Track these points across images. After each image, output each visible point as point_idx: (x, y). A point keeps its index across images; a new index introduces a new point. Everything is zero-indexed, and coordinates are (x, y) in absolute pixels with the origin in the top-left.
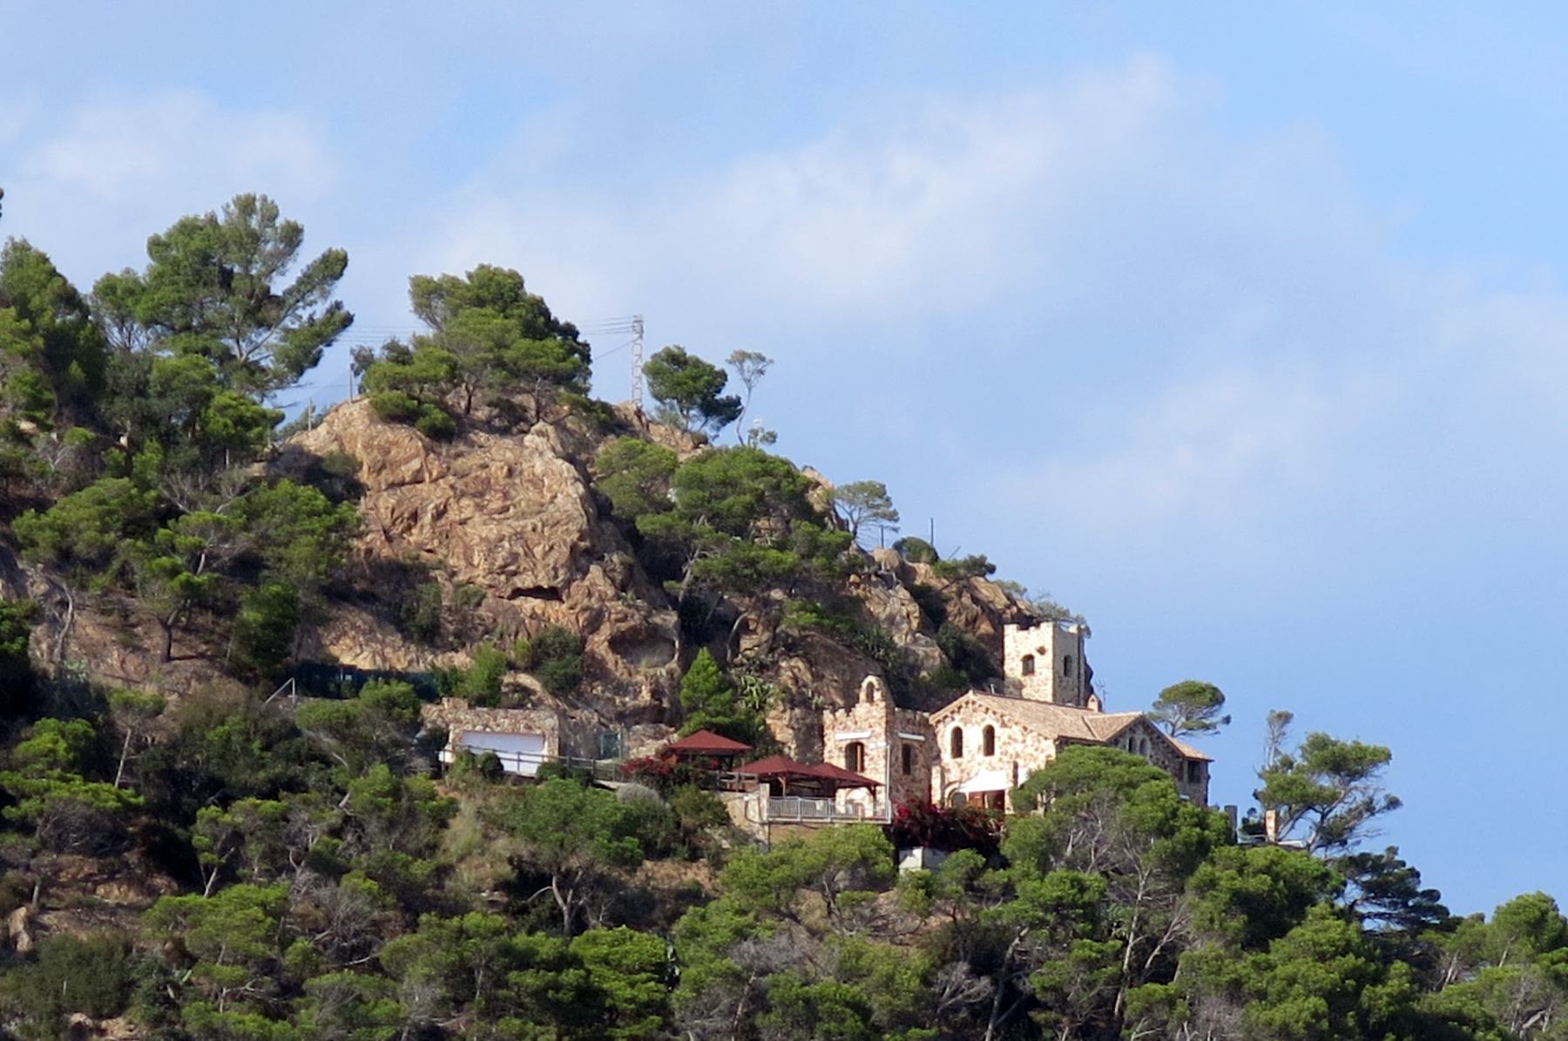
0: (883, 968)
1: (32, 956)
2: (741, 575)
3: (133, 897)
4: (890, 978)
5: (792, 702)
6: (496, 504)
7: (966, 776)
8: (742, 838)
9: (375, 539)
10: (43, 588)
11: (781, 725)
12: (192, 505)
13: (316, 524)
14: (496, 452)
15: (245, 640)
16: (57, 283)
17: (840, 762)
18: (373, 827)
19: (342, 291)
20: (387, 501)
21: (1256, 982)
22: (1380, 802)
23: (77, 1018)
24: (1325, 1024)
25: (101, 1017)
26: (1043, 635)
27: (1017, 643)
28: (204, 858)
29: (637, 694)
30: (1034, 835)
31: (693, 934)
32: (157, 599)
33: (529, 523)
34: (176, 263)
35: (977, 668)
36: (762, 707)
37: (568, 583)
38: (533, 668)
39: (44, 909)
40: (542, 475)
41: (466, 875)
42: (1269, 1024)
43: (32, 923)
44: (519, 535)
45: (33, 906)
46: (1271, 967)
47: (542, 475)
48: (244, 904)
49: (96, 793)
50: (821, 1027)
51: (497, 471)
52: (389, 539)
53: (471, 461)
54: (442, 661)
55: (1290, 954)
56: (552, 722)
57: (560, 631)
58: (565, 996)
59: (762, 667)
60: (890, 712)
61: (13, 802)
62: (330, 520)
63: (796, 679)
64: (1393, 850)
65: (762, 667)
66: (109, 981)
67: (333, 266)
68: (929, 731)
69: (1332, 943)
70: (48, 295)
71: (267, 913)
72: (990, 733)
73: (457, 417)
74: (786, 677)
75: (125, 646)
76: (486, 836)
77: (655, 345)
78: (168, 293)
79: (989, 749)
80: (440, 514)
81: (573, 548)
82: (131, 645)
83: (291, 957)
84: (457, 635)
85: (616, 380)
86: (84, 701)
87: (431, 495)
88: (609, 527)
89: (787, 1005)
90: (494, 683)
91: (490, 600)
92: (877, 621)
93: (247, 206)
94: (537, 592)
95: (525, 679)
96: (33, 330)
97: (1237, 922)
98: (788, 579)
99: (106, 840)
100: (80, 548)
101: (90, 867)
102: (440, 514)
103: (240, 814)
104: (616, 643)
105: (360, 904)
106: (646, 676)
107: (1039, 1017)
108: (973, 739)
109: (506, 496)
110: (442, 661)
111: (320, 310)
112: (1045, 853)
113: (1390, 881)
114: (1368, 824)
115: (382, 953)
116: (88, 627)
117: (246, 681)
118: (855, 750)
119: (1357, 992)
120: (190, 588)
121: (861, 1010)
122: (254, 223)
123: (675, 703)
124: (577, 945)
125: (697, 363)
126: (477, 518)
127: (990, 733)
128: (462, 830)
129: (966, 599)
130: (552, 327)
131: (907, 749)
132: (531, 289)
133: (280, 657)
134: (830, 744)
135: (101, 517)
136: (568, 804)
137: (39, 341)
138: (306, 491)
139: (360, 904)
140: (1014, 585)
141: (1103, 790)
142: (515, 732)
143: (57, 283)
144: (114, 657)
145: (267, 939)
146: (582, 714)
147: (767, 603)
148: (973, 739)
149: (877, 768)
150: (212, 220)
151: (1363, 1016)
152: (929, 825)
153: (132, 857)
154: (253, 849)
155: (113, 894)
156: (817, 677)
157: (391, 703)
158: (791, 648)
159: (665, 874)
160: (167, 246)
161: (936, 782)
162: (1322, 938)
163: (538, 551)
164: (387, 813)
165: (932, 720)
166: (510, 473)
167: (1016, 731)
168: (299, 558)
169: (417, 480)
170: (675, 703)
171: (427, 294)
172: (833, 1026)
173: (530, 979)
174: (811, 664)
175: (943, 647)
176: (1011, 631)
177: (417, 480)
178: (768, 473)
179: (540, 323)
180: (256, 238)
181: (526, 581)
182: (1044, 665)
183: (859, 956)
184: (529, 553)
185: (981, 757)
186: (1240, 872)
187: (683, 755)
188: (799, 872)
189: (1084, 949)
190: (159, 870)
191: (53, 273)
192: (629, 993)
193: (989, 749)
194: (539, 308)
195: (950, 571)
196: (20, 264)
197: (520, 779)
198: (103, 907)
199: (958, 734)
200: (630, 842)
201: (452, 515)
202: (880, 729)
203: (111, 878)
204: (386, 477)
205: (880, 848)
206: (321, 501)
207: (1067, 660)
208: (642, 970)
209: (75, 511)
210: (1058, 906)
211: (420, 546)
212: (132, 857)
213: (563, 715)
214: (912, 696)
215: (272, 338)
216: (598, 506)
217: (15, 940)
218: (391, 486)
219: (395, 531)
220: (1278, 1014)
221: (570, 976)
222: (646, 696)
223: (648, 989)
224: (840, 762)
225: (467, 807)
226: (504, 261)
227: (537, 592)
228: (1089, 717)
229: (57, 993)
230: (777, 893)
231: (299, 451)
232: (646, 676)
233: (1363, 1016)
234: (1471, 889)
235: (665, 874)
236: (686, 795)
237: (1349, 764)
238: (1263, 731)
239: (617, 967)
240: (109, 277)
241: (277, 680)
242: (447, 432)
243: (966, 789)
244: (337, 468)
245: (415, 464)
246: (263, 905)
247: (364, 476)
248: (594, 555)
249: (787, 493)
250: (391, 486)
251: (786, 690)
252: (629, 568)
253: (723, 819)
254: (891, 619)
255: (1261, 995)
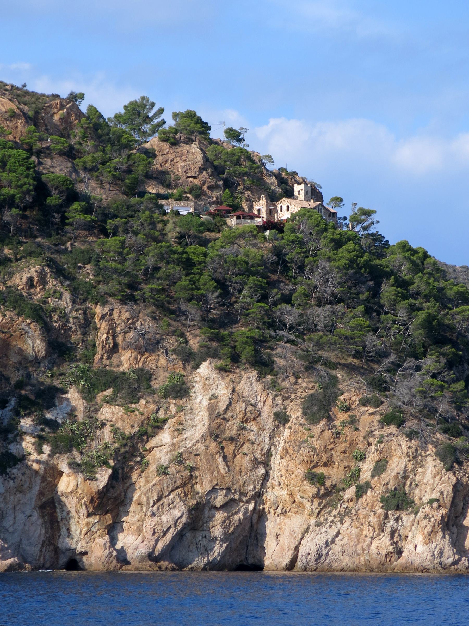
0: (253, 254)
1: (71, 252)
2: (237, 173)
3: (95, 239)
4: (255, 256)
5: (247, 200)
6: (184, 159)
7: (283, 215)
8: (231, 228)
9: (158, 166)
10: (83, 176)
11: (245, 205)
12: (116, 158)
13: (144, 162)
14: (185, 148)
15: (127, 187)
16: (98, 113)
17: (256, 213)
18: (145, 224)
19: (163, 116)
20: (161, 158)
21: (333, 257)
22: (375, 221)
23: (79, 264)
24: (347, 266)
25: (85, 264)
26: (302, 186)
27: (297, 188)
28: (109, 231)
29: (213, 198)
30: (290, 227)
31: (212, 247)
32: (107, 178)
33: (191, 162)
34: (129, 110)
35: (289, 194)
36: (241, 201)
37: (198, 175)
38: (190, 193)
39: (75, 242)
40: (194, 152)
41: (170, 235)
42: (335, 266)
43: (72, 245)
44: (188, 165)
45: (72, 241)
46: (337, 254)
47: (194, 152)
48: (115, 240)
49: (85, 217)
50: (237, 266)
51: (185, 152)
52: (161, 166)
53: (179, 150)
54: (170, 191)
55: (342, 252)
56: (193, 204)
57: (196, 185)
58: (183, 260)
59: (241, 193)
60: (267, 202)
61: (68, 219)
62: (147, 162)
63: (248, 196)
64: (377, 232)
65: (241, 193)
66: (87, 257)
67: (161, 111)
68: (276, 206)
69: (351, 249)
70: (96, 116)
71: (120, 242)
72: (288, 206)
73: (178, 141)
74: (246, 195)
75: (101, 188)
76: (175, 227)
77: (227, 127)
78: (127, 117)
79: (288, 210)
80: (172, 161)
81: (200, 168)
82: (102, 188)
83: (125, 252)
84: (175, 186)
85: (217, 133)
86: (87, 198)
87: (170, 157)
88: (208, 163)
89: (230, 262)
90: (180, 196)
91: (182, 179)
92: (268, 184)
93: (143, 98)
94: (192, 177)
95: (188, 195)
96: (90, 123)
97: (331, 245)
98: (246, 174)
99: (89, 227)
100: (88, 166)
101: (86, 233)
102: (172, 161)
103: (116, 222)
104: (209, 188)
105: (141, 241)
106: (215, 195)
107: (289, 265)
108: (285, 208)
109: (186, 157)
110: (170, 191)
111: (159, 120)
112: (293, 231)
113: (377, 238)
114: (372, 226)
115: (145, 251)
116: (93, 184)
117: (127, 195)
118: (259, 210)
119: (357, 260)
120: (114, 176)
121: (247, 263)
122: (144, 102)
123: (221, 200)
124: (187, 249)
125: (235, 130)
126: (180, 161)
127: (288, 206)
128: (170, 226)
129: (293, 180)
130: (202, 122)
131: (271, 210)
132: (198, 114)
133: (135, 189)
134: (254, 209)
135: (92, 160)
136: (189, 220)
137: (91, 125)
138: (142, 155)
139: (141, 241)
140: (305, 178)
141: (306, 217)
142: (184, 206)
143: (98, 113)
144: (98, 190)
145: (120, 248)
146: (200, 203)
147: (244, 180)
148: (285, 208)
149: (264, 214)
150: (136, 102)
151: (358, 265)
152: (270, 225)
153: (96, 231)
154: (120, 229)
155: (90, 239)
156: (253, 195)
157: (150, 199)
158: (248, 189)
159: (208, 235)
160: (127, 107)
161: (276, 217)
162: (349, 248)
163: (192, 168)
164: (148, 222)
165: (276, 204)
166: (188, 152)
167: (293, 206)
168: (140, 170)
169: (168, 153)
170: (221, 200)
171: (175, 115)
172: (240, 266)
173: (176, 256)
174: (252, 192)
175: (283, 190)
176: (296, 185)
177: (168, 153)
178: (242, 152)
179: (199, 121)
180: (145, 106)
181: (189, 175)
182: (302, 193)
183: (248, 252)
184: (190, 169)
185: (286, 212)
186: (333, 235)
187: (218, 210)
188: (237, 234)
189: (298, 250)
190: (101, 234)
191: (98, 111)
192: (197, 259)
193: (288, 210)
194: (199, 118)
195: (288, 174)
196: (91, 109)
197: (184, 216)
198: (88, 242)
199: (281, 207)
200: (201, 228)
201: (175, 161)
202: (265, 206)
203: (91, 236)
204: (161, 153)
205: (255, 229)
206: (145, 158)
207: (307, 192)
208: (201, 254)
209: (88, 159)
210: (293, 242)
211: (168, 167)
212: (96, 231)
213: (195, 202)
214: (273, 198)
215: (149, 126)
216: (206, 159)
217: (68, 248)
218: (162, 155)
219: (163, 164)
220: (337, 264)
221: (185, 256)
222: (215, 199)
223: (201, 258)
224: (256, 213)
225: (171, 221)
226: (192, 109)
227: (192, 177)
228: (310, 203)
229: (76, 259)
230: (233, 239)
231: (144, 148)
232: (215, 195)
233: (358, 265)
234: (393, 239)
235: (208, 235)
236: (218, 219)
237: (368, 213)
238: (351, 207)
239: (195, 254)
240: (116, 114)
241: (133, 195)
242: (175, 143)
243: (283, 218)
244: (151, 151)
245: (167, 150)
246: (120, 241)
247: (156, 153)
248: (204, 169)
249: (249, 157)
250: (162, 155)
251: (246, 198)
252: (212, 172)
253: (225, 224)
254: (271, 183)
255: (334, 260)
